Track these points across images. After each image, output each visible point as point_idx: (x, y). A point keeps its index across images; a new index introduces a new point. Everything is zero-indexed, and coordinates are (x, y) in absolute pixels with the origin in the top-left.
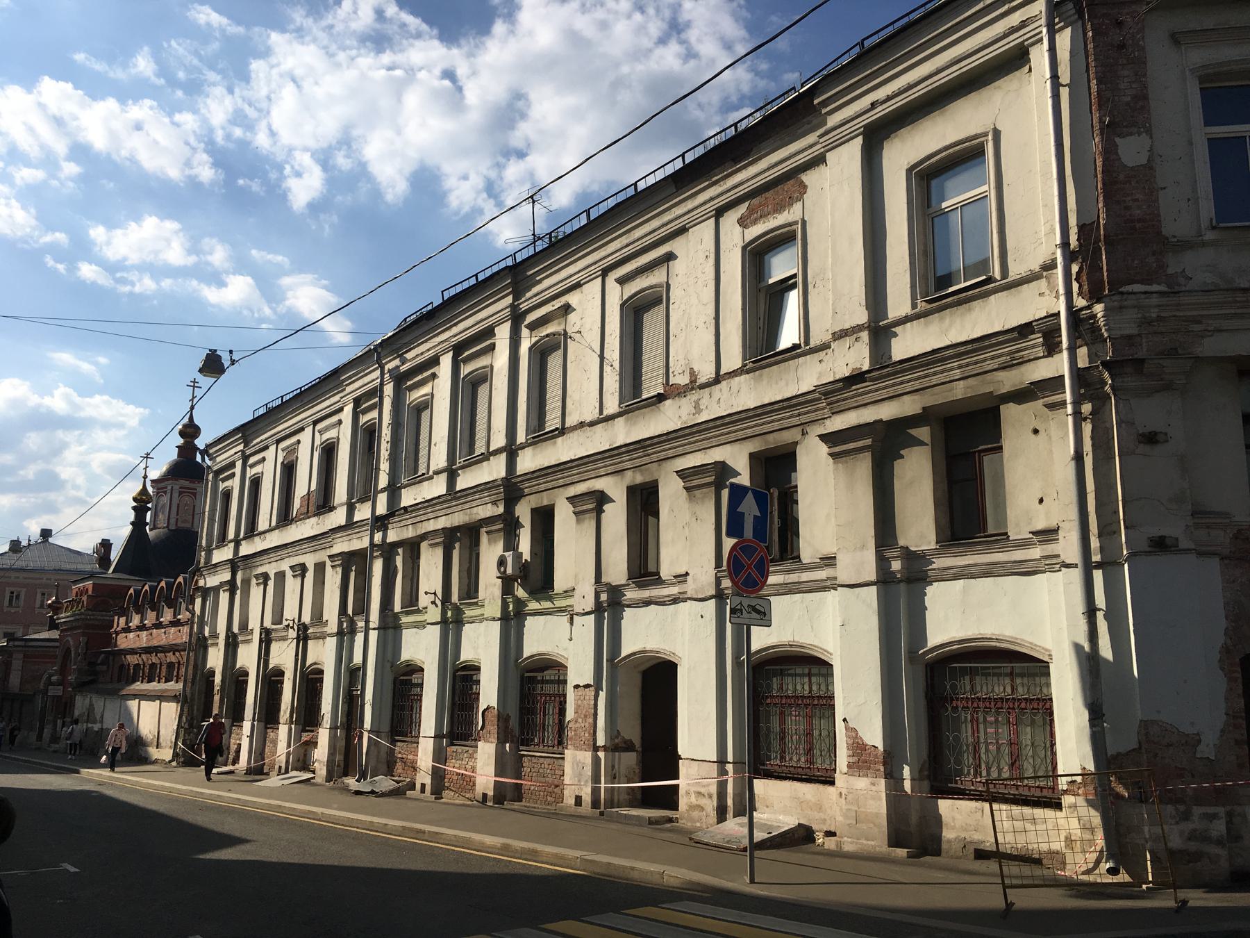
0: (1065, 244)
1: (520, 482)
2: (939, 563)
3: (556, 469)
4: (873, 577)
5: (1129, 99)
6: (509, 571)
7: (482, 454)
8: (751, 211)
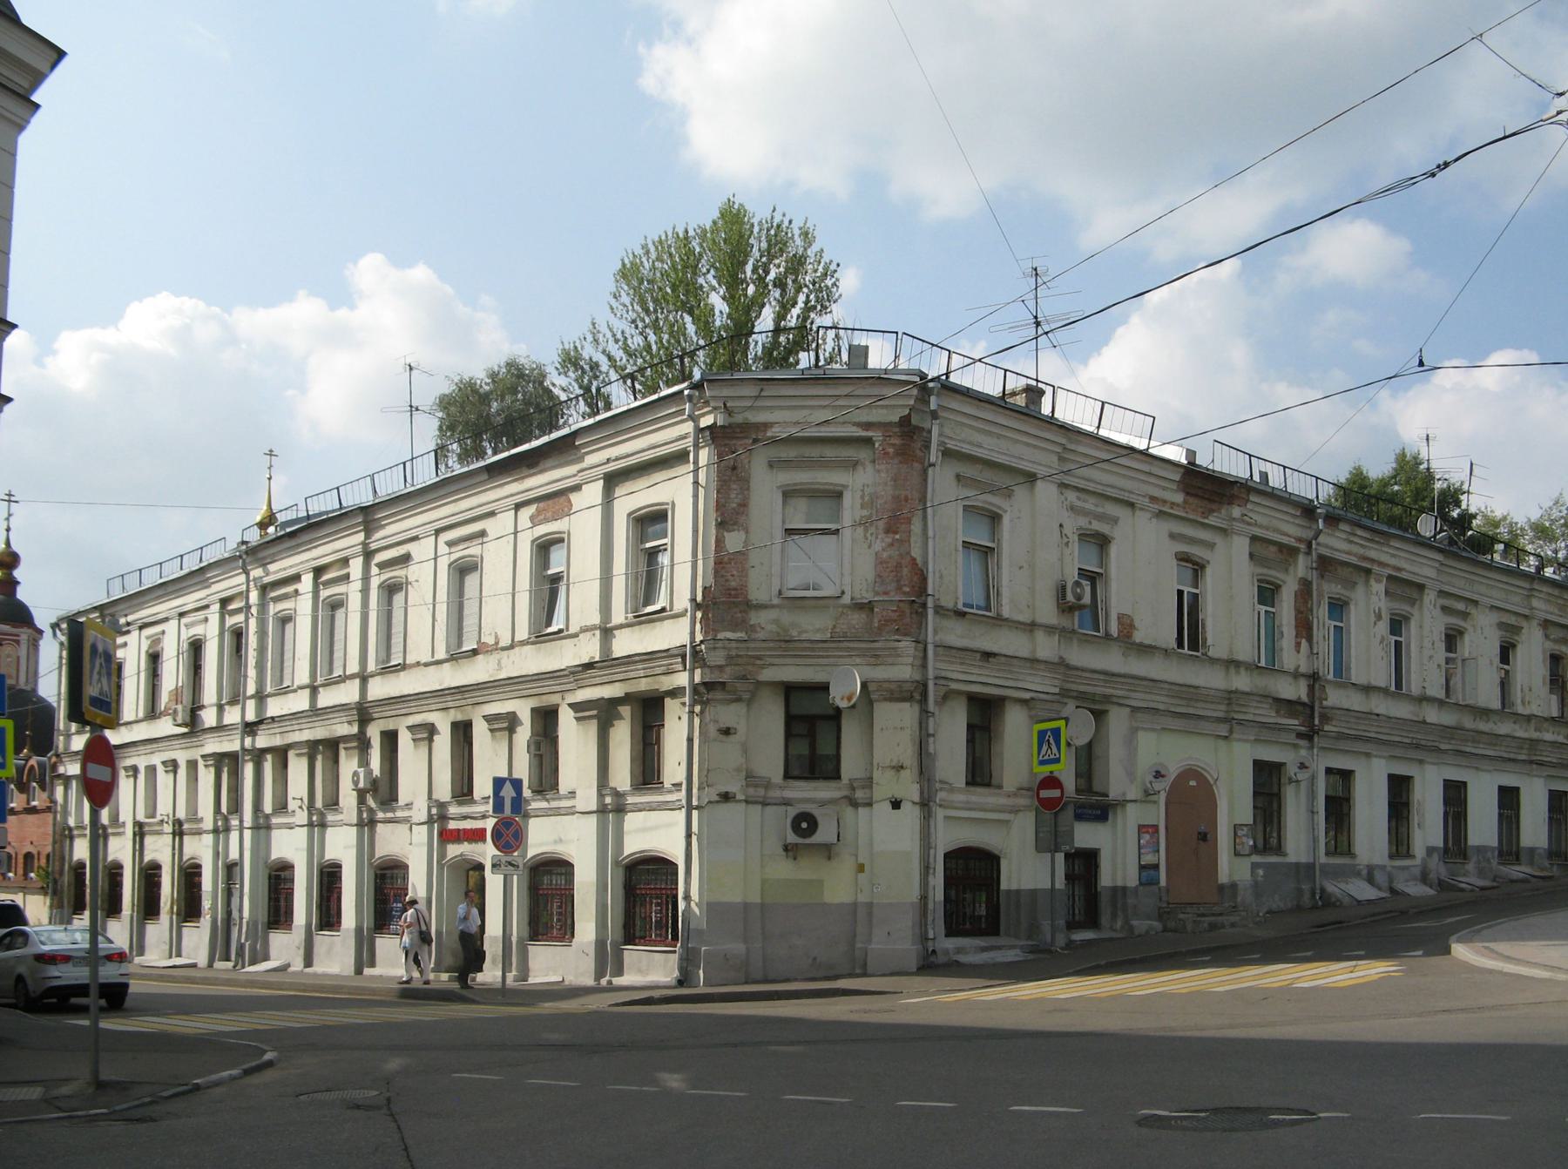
0: (693, 600)
1: (370, 707)
2: (630, 800)
3: (399, 700)
4: (355, 822)
5: (735, 505)
6: (361, 785)
7: (340, 676)
8: (539, 512)
